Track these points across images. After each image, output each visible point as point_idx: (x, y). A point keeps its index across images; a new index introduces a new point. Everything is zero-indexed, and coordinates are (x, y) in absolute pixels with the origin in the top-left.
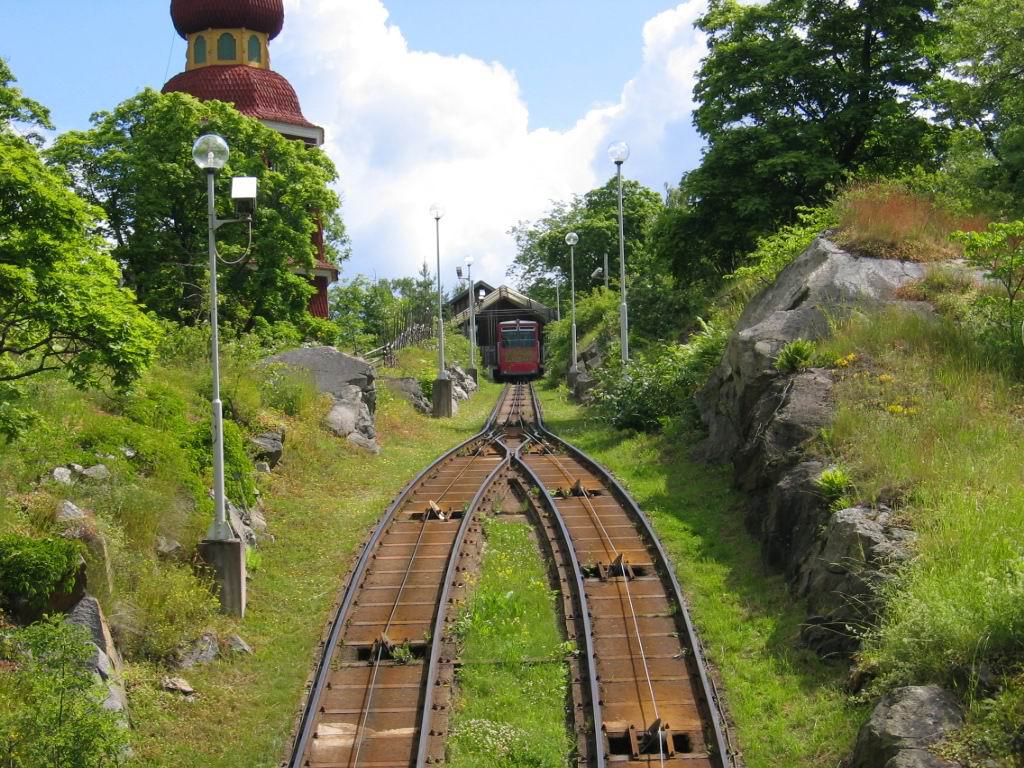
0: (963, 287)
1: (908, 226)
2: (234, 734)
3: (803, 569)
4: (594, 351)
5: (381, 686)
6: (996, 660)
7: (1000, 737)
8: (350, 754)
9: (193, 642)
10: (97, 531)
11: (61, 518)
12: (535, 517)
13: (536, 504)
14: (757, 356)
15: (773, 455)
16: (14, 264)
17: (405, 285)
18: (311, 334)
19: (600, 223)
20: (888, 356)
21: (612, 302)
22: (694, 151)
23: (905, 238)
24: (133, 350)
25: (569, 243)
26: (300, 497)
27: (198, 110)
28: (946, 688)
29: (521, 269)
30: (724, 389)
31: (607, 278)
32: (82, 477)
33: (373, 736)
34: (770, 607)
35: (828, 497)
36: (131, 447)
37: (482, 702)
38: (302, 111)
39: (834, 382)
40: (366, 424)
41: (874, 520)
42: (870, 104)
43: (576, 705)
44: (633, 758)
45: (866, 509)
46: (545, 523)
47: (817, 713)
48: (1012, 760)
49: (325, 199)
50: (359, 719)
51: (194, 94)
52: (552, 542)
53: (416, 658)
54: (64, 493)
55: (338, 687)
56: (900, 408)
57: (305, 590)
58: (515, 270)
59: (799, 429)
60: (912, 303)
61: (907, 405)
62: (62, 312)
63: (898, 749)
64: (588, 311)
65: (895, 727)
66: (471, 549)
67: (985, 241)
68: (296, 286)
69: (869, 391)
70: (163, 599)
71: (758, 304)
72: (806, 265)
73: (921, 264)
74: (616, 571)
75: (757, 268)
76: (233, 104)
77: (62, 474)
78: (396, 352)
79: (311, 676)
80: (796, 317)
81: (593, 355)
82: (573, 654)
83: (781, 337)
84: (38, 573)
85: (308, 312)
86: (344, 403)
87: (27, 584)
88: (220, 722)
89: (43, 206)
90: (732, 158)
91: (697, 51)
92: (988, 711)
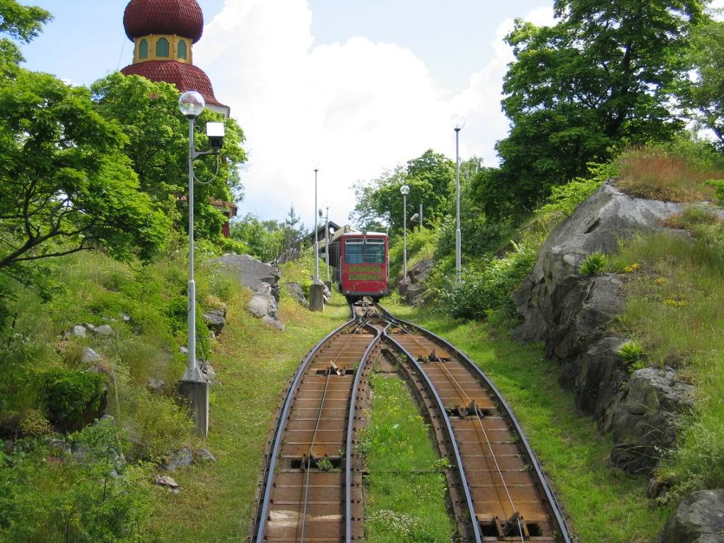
2: (210, 516)
3: (608, 412)
4: (418, 270)
5: (312, 486)
8: (296, 532)
9: (176, 452)
11: (85, 359)
12: (405, 375)
13: (405, 366)
14: (565, 264)
15: (582, 332)
16: (74, 168)
18: (228, 249)
21: (428, 238)
22: (503, 127)
24: (155, 233)
25: (403, 193)
26: (235, 357)
27: (151, 88)
29: (357, 216)
30: (536, 290)
32: (94, 333)
33: (311, 520)
34: (584, 437)
35: (626, 363)
36: (127, 313)
37: (386, 498)
38: (215, 94)
39: (624, 283)
40: (274, 310)
42: (628, 97)
43: (454, 502)
44: (501, 539)
45: (657, 370)
46: (414, 379)
47: (628, 511)
49: (238, 154)
50: (299, 508)
51: (148, 78)
52: (421, 392)
53: (335, 468)
55: (281, 486)
57: (248, 419)
59: (601, 314)
62: (105, 205)
63: (699, 534)
64: (410, 243)
65: (696, 519)
66: (364, 395)
69: (650, 289)
72: (596, 203)
74: (471, 412)
76: (175, 85)
77: (80, 330)
79: (261, 478)
81: (417, 273)
82: (448, 468)
83: (582, 252)
84: (74, 396)
85: (222, 235)
87: (67, 403)
88: (198, 508)
89: (95, 127)
90: (532, 131)
91: (506, 57)
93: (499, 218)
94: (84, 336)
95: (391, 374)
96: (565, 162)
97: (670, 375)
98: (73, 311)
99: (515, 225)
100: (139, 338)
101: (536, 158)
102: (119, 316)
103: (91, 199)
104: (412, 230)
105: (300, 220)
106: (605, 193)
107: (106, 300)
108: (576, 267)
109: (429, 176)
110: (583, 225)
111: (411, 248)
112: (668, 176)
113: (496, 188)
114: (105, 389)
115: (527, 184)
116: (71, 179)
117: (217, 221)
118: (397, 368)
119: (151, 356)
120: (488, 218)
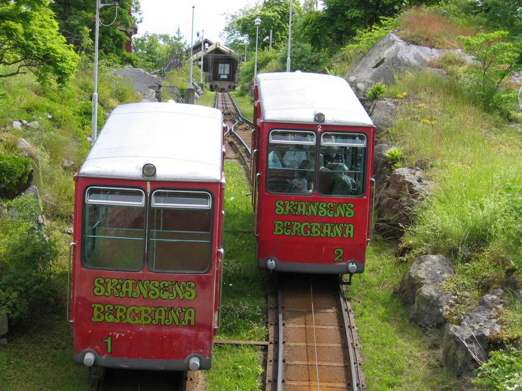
0: (461, 63)
1: (434, 30)
6: (471, 245)
7: (472, 281)
10: (36, 154)
11: (20, 146)
12: (243, 162)
13: (244, 155)
17: (165, 38)
19: (269, 13)
20: (422, 95)
23: (434, 36)
28: (446, 257)
29: (226, 34)
31: (271, 42)
32: (27, 127)
35: (390, 163)
36: (50, 113)
39: (396, 105)
41: (414, 174)
45: (410, 169)
47: (381, 265)
48: (477, 293)
54: (17, 133)
56: (428, 121)
58: (223, 34)
60: (435, 69)
61: (431, 120)
62: (34, 46)
64: (262, 58)
65: (422, 274)
67: (474, 42)
68: (119, 36)
70: (66, 190)
71: (358, 63)
72: (383, 46)
73: (440, 50)
75: (358, 46)
78: (166, 73)
80: (378, 72)
83: (370, 81)
84: (10, 173)
86: (147, 98)
87: (5, 178)
92: (467, 269)
93: (320, 49)
94: (20, 128)
95: (234, 160)
96: (368, 12)
97: (418, 173)
98: (12, 111)
99: (331, 55)
100: (58, 131)
101: (348, 8)
102: (45, 116)
103: (25, 41)
104: (263, 49)
105: (184, 37)
106: (390, 40)
107: (36, 104)
108: (365, 92)
109: (279, 9)
110: (372, 62)
111: (261, 62)
112: (434, 30)
113: (319, 28)
114: (32, 168)
115: (341, 26)
116: (11, 29)
117: (121, 40)
118: (238, 155)
119: (65, 145)
120: (313, 47)
